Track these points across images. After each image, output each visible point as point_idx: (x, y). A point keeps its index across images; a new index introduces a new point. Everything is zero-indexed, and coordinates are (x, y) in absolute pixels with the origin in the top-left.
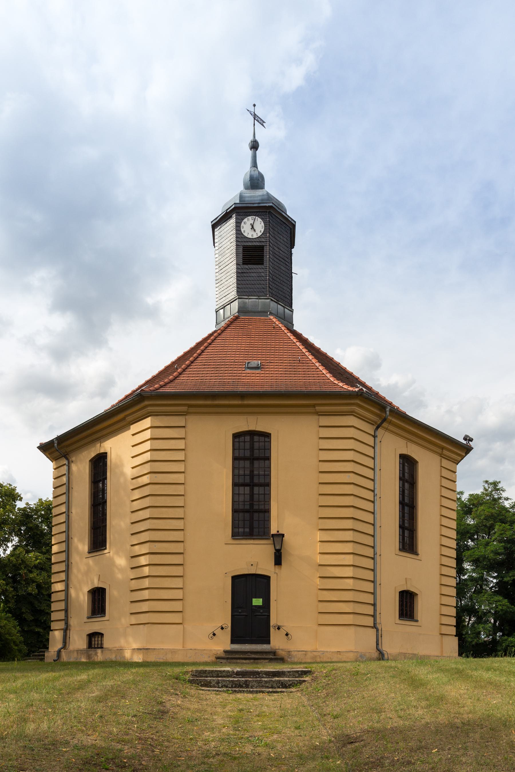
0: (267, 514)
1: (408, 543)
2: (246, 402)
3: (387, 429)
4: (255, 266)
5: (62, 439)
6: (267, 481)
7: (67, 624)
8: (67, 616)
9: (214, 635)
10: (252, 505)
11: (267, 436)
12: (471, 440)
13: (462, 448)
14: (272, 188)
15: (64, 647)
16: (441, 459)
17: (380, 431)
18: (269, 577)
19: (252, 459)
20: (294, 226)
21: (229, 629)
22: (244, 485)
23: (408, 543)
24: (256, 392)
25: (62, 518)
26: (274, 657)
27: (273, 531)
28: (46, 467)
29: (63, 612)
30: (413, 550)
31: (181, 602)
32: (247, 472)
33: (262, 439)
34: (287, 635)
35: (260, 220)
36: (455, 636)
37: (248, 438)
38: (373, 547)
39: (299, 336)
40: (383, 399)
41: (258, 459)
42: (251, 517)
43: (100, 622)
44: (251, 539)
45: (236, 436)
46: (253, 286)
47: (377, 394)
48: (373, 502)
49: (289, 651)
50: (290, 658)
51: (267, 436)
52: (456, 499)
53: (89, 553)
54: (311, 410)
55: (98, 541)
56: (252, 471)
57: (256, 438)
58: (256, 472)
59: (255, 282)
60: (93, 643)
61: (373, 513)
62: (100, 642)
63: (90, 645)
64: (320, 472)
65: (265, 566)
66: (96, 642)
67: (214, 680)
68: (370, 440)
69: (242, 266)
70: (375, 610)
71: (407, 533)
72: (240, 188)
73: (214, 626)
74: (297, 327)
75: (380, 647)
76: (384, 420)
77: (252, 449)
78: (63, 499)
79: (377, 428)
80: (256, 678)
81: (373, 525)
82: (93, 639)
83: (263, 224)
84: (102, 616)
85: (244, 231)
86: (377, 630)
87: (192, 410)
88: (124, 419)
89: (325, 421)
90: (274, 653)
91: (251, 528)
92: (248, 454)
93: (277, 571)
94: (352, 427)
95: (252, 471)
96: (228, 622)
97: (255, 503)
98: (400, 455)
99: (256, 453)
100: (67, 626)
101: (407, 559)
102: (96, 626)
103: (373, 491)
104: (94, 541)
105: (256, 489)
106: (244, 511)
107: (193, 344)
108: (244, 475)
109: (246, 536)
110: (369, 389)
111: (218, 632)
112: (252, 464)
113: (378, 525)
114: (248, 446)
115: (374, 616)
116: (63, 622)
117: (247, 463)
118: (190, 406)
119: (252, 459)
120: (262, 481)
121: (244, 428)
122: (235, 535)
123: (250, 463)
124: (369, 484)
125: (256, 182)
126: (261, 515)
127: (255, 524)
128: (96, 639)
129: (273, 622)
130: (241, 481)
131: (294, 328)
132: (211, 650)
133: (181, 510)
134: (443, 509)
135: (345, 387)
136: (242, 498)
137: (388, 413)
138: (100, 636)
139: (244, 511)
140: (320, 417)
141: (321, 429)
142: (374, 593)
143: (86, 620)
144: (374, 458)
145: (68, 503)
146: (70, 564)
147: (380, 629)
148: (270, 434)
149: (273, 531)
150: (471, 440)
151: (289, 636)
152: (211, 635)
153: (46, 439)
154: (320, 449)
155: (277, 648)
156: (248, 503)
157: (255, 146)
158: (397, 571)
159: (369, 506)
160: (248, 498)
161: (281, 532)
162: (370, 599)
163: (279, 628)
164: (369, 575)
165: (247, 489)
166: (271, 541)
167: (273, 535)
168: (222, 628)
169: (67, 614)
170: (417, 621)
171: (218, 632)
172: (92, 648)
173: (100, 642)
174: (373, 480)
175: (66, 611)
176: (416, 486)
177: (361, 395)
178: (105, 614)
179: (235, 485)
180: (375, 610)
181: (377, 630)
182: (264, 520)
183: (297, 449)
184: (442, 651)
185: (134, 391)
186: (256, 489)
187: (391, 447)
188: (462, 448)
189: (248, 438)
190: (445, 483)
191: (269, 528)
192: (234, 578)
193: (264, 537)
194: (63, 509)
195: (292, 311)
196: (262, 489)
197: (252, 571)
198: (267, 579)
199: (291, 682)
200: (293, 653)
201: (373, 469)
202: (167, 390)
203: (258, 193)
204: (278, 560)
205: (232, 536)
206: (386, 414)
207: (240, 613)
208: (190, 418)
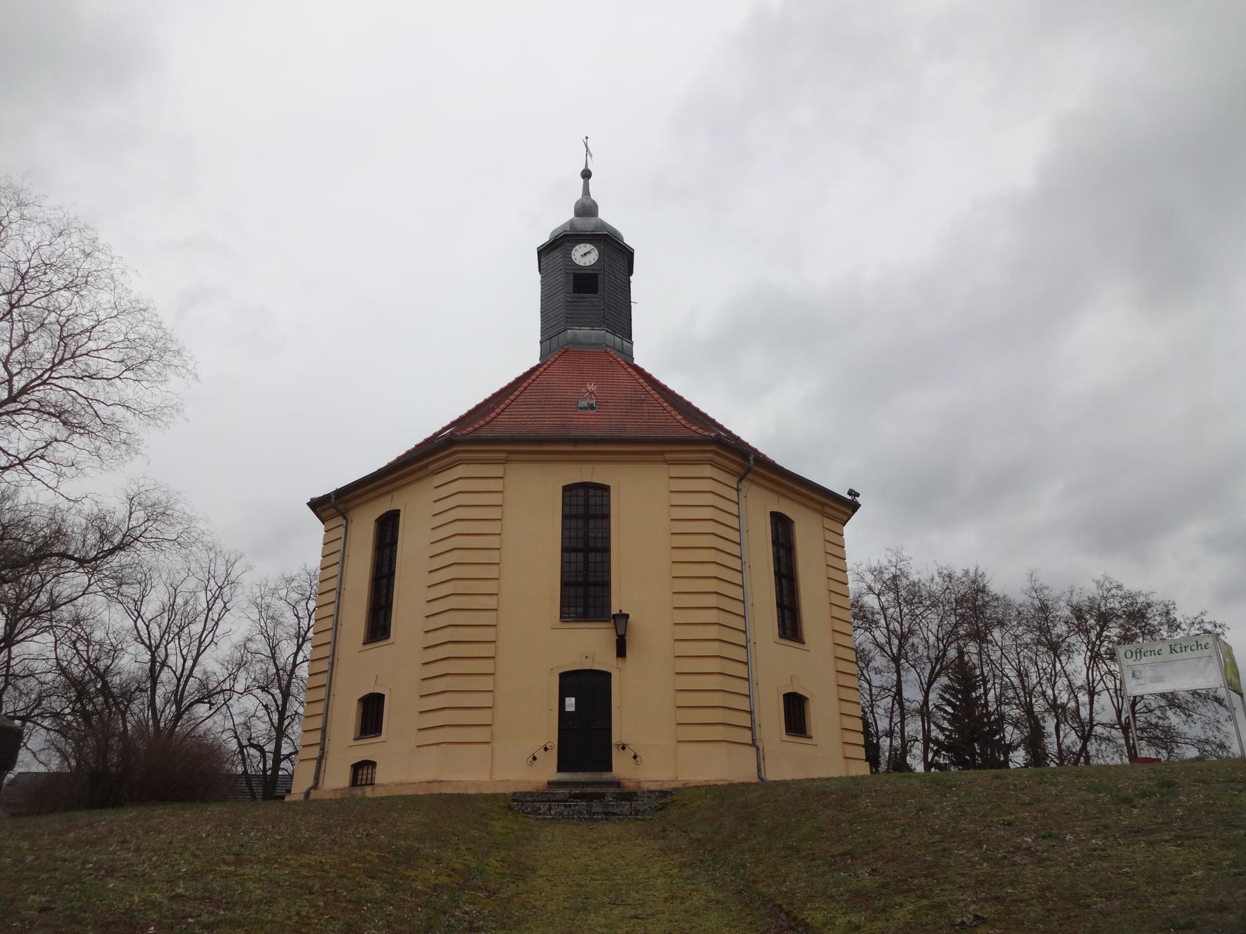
0: (605, 554)
2: (579, 448)
5: (342, 493)
7: (322, 749)
8: (323, 739)
9: (535, 758)
11: (605, 489)
12: (858, 495)
13: (846, 506)
14: (609, 215)
17: (745, 485)
19: (586, 517)
20: (632, 254)
27: (615, 610)
28: (315, 529)
31: (490, 711)
32: (581, 534)
33: (599, 493)
34: (635, 757)
37: (581, 492)
38: (745, 632)
39: (640, 371)
40: (746, 444)
41: (594, 517)
42: (586, 588)
45: (567, 489)
47: (738, 438)
51: (605, 489)
53: (364, 644)
54: (660, 457)
56: (586, 533)
57: (592, 492)
58: (591, 534)
61: (742, 587)
63: (354, 782)
68: (733, 495)
70: (753, 721)
71: (785, 582)
73: (535, 745)
74: (638, 361)
76: (749, 470)
77: (587, 505)
79: (740, 480)
81: (743, 602)
86: (758, 749)
88: (426, 466)
89: (676, 471)
90: (618, 784)
92: (581, 510)
94: (706, 481)
95: (586, 533)
96: (553, 738)
99: (592, 511)
101: (789, 650)
102: (367, 750)
103: (740, 558)
105: (592, 555)
107: (511, 379)
110: (729, 433)
111: (540, 754)
113: (749, 602)
114: (581, 500)
117: (581, 523)
118: (510, 452)
119: (586, 518)
121: (577, 479)
122: (564, 617)
124: (735, 550)
125: (586, 209)
129: (615, 739)
133: (496, 553)
134: (837, 635)
135: (700, 431)
141: (673, 495)
149: (614, 611)
150: (858, 495)
153: (319, 493)
157: (586, 175)
158: (779, 667)
160: (581, 567)
162: (745, 720)
163: (623, 748)
164: (745, 720)
166: (611, 624)
168: (546, 749)
170: (811, 737)
171: (540, 754)
180: (753, 721)
181: (758, 749)
183: (645, 505)
185: (436, 435)
187: (759, 506)
188: (846, 506)
189: (581, 492)
195: (632, 343)
197: (587, 666)
198: (607, 676)
201: (739, 530)
202: (483, 433)
203: (592, 220)
204: (621, 652)
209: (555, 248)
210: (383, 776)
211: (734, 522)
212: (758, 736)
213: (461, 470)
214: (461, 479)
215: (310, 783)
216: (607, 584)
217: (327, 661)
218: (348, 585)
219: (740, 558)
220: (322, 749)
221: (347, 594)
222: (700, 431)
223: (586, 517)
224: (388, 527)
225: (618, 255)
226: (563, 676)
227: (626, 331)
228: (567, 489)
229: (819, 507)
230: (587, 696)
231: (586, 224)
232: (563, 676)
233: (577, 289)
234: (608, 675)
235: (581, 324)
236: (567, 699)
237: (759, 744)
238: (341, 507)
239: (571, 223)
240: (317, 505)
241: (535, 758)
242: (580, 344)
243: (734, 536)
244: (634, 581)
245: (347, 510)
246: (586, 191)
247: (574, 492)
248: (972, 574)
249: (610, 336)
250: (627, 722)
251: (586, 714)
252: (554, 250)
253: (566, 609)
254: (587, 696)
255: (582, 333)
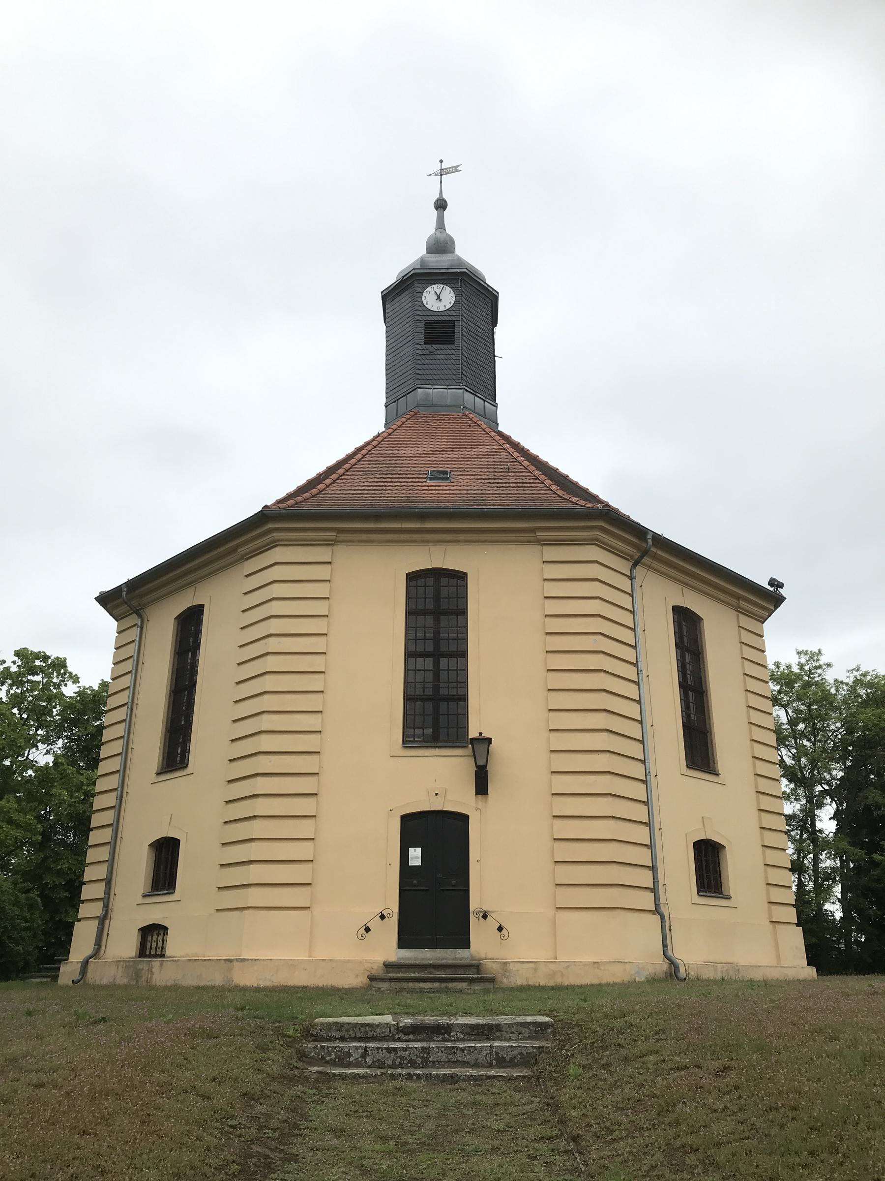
1: (699, 752)
3: (650, 567)
4: (441, 346)
5: (134, 585)
6: (461, 692)
7: (106, 907)
8: (108, 892)
9: (368, 930)
10: (436, 688)
11: (460, 577)
12: (781, 585)
13: (769, 598)
14: (470, 252)
15: (96, 954)
16: (738, 616)
17: (639, 571)
18: (468, 817)
19: (438, 613)
21: (396, 918)
22: (425, 655)
23: (699, 752)
24: (442, 480)
25: (121, 714)
26: (476, 975)
29: (103, 884)
30: (709, 766)
32: (430, 635)
33: (453, 581)
34: (500, 929)
35: (448, 289)
36: (798, 925)
41: (447, 612)
42: (435, 709)
43: (164, 905)
44: (436, 747)
45: (412, 577)
46: (439, 372)
48: (637, 683)
49: (505, 963)
50: (507, 977)
51: (460, 577)
52: (767, 679)
55: (175, 755)
56: (437, 633)
57: (444, 581)
59: (442, 367)
60: (149, 945)
62: (160, 944)
63: (143, 952)
64: (547, 633)
65: (458, 797)
66: (154, 944)
67: (357, 1048)
68: (625, 584)
69: (424, 346)
70: (655, 878)
72: (422, 251)
73: (368, 912)
75: (670, 953)
76: (645, 553)
77: (437, 597)
78: (126, 681)
79: (635, 565)
80: (444, 1040)
81: (641, 722)
82: (149, 939)
83: (453, 294)
84: (169, 893)
85: (427, 303)
86: (663, 918)
87: (342, 536)
88: (234, 550)
89: (552, 553)
90: (476, 967)
91: (436, 727)
93: (480, 805)
94: (595, 565)
95: (437, 633)
97: (441, 685)
98: (673, 607)
99: (444, 606)
100: (107, 911)
101: (699, 782)
103: (636, 665)
104: (168, 753)
105: (443, 662)
106: (423, 699)
108: (425, 639)
109: (427, 742)
112: (437, 620)
113: (648, 723)
114: (430, 591)
115: (654, 890)
116: (100, 904)
118: (339, 531)
119: (437, 614)
120: (453, 648)
122: (408, 741)
123: (434, 620)
124: (628, 654)
125: (441, 245)
126: (453, 705)
127: (443, 720)
128: (155, 938)
129: (474, 904)
130: (420, 648)
131: (499, 429)
132: (361, 962)
135: (582, 502)
136: (420, 677)
137: (650, 541)
138: (162, 932)
139: (423, 699)
140: (545, 548)
142: (650, 847)
143: (140, 900)
144: (633, 612)
145: (133, 689)
146: (125, 794)
147: (667, 916)
148: (466, 574)
150: (781, 585)
151: (504, 931)
152: (363, 931)
153: (155, 769)
154: (546, 598)
155: (483, 956)
156: (431, 685)
157: (441, 205)
158: (689, 808)
159: (631, 691)
160: (430, 676)
161: (486, 735)
163: (485, 916)
165: (429, 662)
166: (468, 751)
167: (473, 740)
168: (382, 917)
169: (110, 889)
170: (728, 898)
172: (146, 956)
173: (160, 944)
174: (634, 647)
175: (108, 881)
176: (703, 658)
177: (607, 513)
178: (174, 889)
179: (409, 655)
180: (655, 878)
181: (663, 918)
182: (458, 715)
183: (510, 602)
184: (778, 957)
186: (443, 662)
188: (769, 598)
189: (430, 581)
190: (749, 653)
191: (466, 728)
192: (405, 819)
193: (457, 744)
194: (123, 698)
196: (453, 661)
197: (437, 805)
199: (516, 1052)
200: (511, 966)
201: (633, 630)
204: (482, 787)
205: (404, 742)
206: (647, 542)
207: (415, 886)
208: (339, 550)
209: (403, 291)
210: (174, 946)
211: (627, 619)
212: (662, 900)
213: (279, 554)
214: (286, 564)
215: (89, 951)
216: (463, 699)
217: (114, 794)
218: (142, 700)
219: (636, 665)
220: (106, 907)
221: (140, 711)
222: (582, 502)
223: (438, 613)
224: (190, 624)
225: (479, 299)
226: (406, 819)
227: (487, 389)
228: (412, 577)
229: (734, 601)
230: (437, 848)
231: (441, 261)
232: (406, 819)
233: (429, 340)
234: (465, 818)
235: (433, 383)
236: (411, 850)
237: (663, 909)
238: (134, 603)
239: (422, 261)
240: (107, 600)
241: (368, 930)
242: (433, 406)
243: (628, 636)
244: (501, 691)
245: (143, 607)
246: (441, 224)
247: (421, 582)
248: (823, 660)
249: (468, 397)
250: (490, 880)
251: (436, 874)
252: (401, 293)
253: (410, 731)
254: (437, 848)
255: (435, 393)
